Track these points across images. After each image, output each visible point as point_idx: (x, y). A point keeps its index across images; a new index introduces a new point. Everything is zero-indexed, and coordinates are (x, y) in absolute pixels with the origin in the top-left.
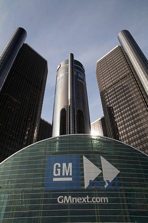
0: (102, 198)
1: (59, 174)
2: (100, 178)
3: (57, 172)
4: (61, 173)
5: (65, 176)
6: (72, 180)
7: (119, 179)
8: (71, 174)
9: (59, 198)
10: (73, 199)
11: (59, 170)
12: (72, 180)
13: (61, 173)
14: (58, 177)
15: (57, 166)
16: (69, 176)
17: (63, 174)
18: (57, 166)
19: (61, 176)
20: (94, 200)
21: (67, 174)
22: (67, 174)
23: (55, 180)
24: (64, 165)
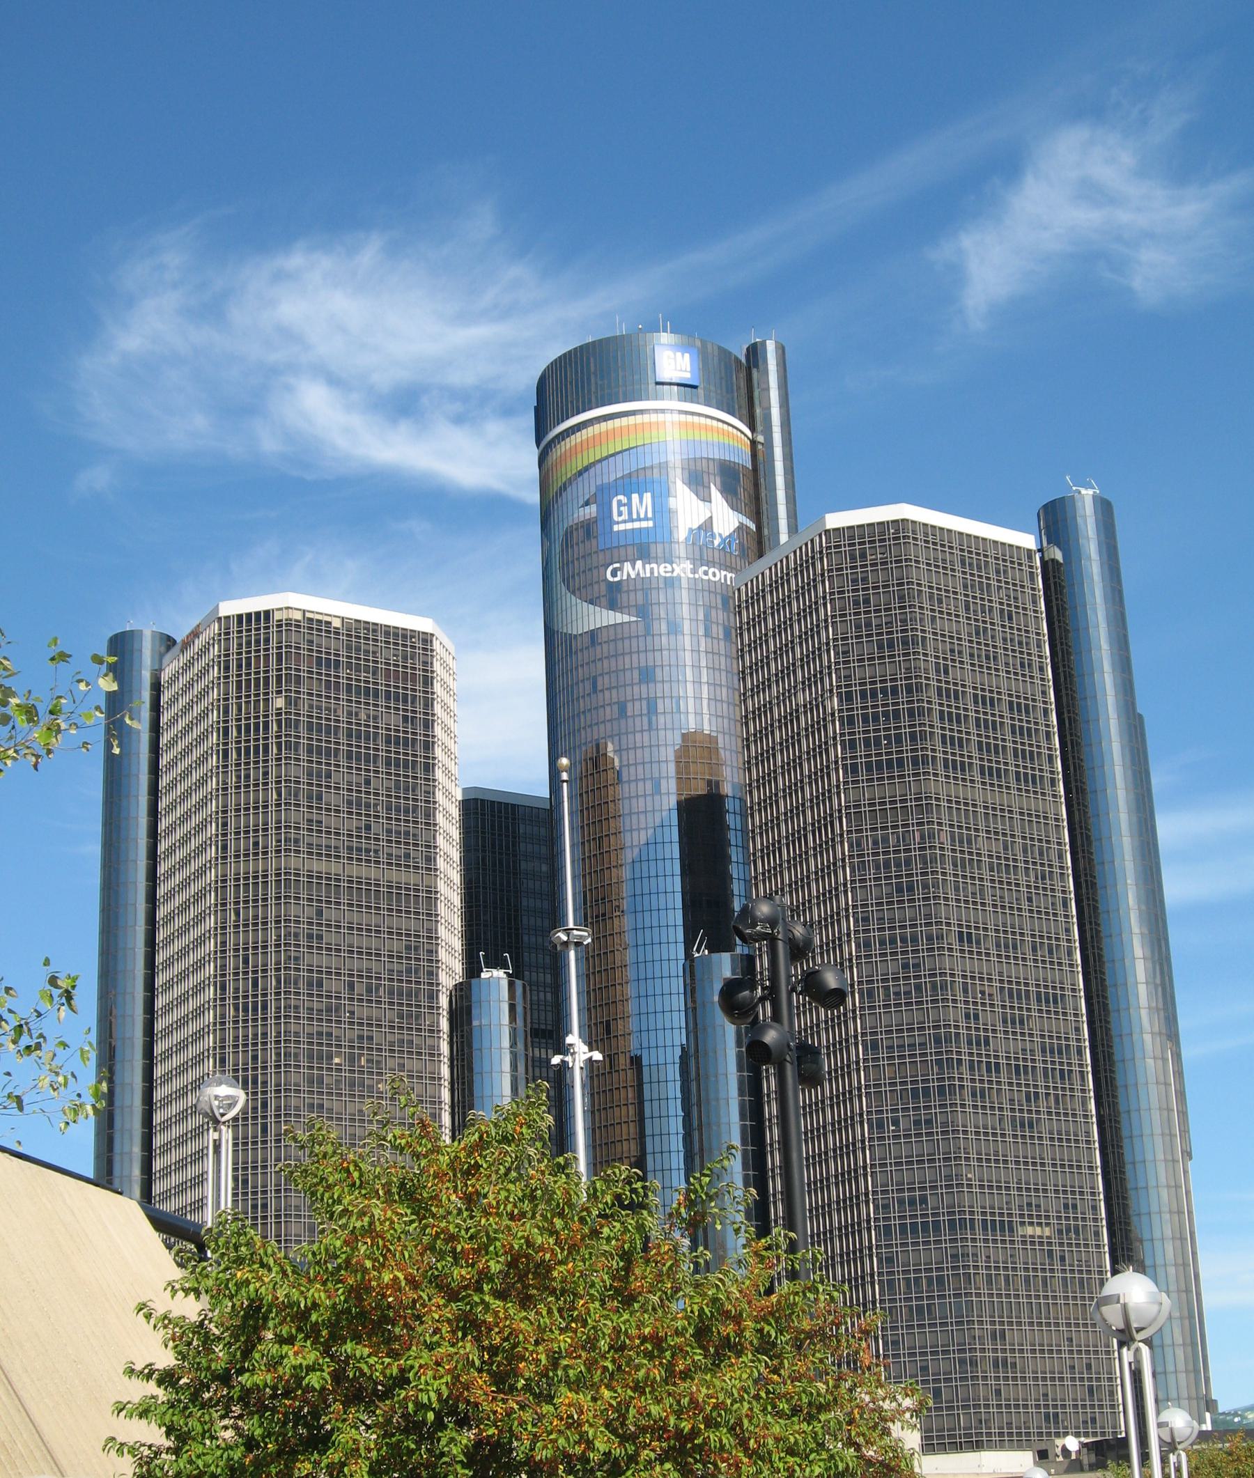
0: (723, 573)
1: (625, 516)
2: (707, 526)
3: (620, 514)
4: (630, 513)
5: (639, 519)
6: (828, 516)
7: (387, 634)
8: (650, 515)
9: (611, 568)
10: (647, 566)
11: (624, 509)
12: (828, 516)
13: (630, 513)
14: (625, 522)
15: (619, 502)
16: (646, 519)
17: (635, 516)
18: (619, 502)
19: (631, 520)
20: (706, 573)
21: (642, 516)
22: (642, 516)
23: (616, 528)
24: (635, 497)
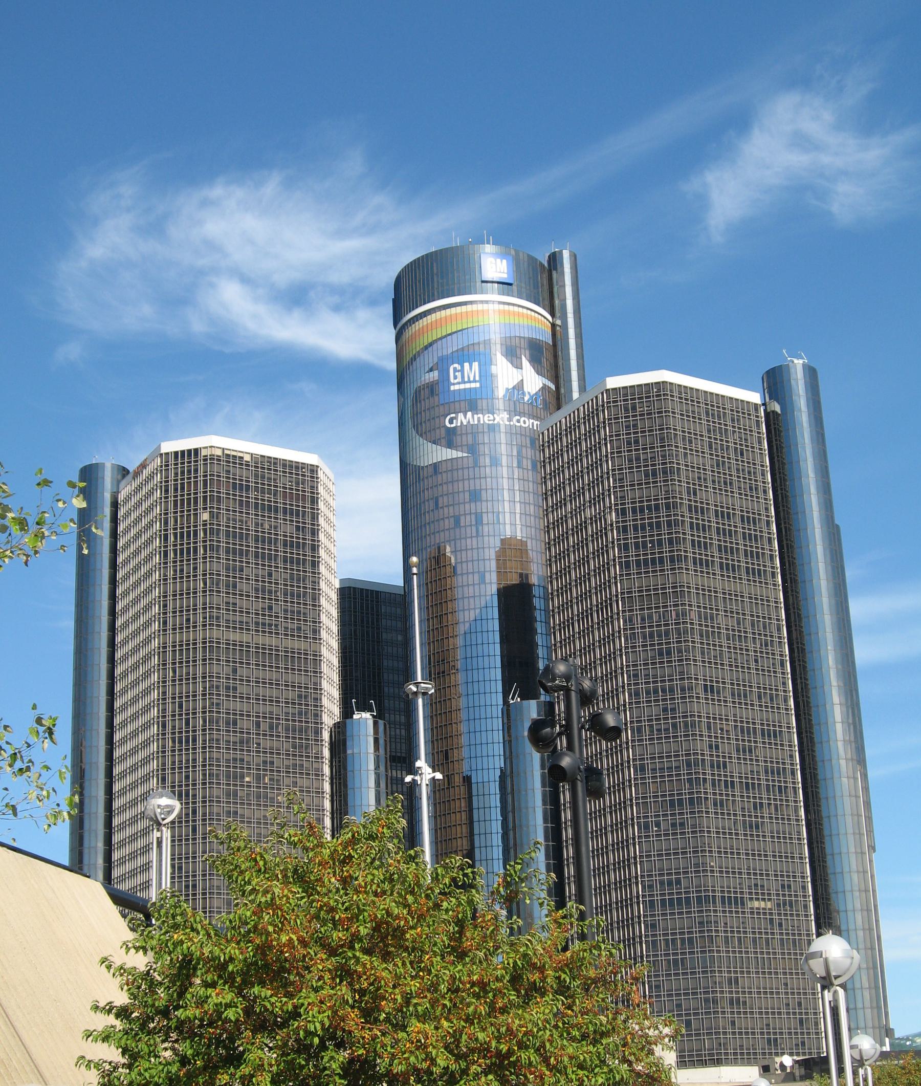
0: (531, 421)
1: (459, 379)
2: (520, 386)
3: (455, 378)
4: (463, 377)
5: (469, 382)
6: (608, 379)
7: (284, 466)
8: (477, 378)
9: (448, 417)
10: (476, 416)
11: (459, 374)
12: (608, 379)
13: (463, 377)
14: (459, 383)
15: (455, 369)
16: (475, 381)
17: (466, 379)
18: (455, 369)
19: (464, 382)
20: (518, 421)
21: (472, 379)
22: (472, 379)
23: (452, 388)
24: (466, 365)
